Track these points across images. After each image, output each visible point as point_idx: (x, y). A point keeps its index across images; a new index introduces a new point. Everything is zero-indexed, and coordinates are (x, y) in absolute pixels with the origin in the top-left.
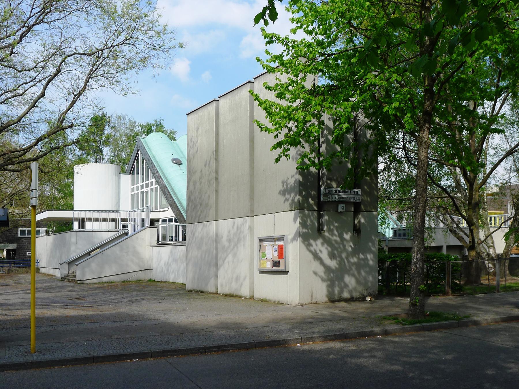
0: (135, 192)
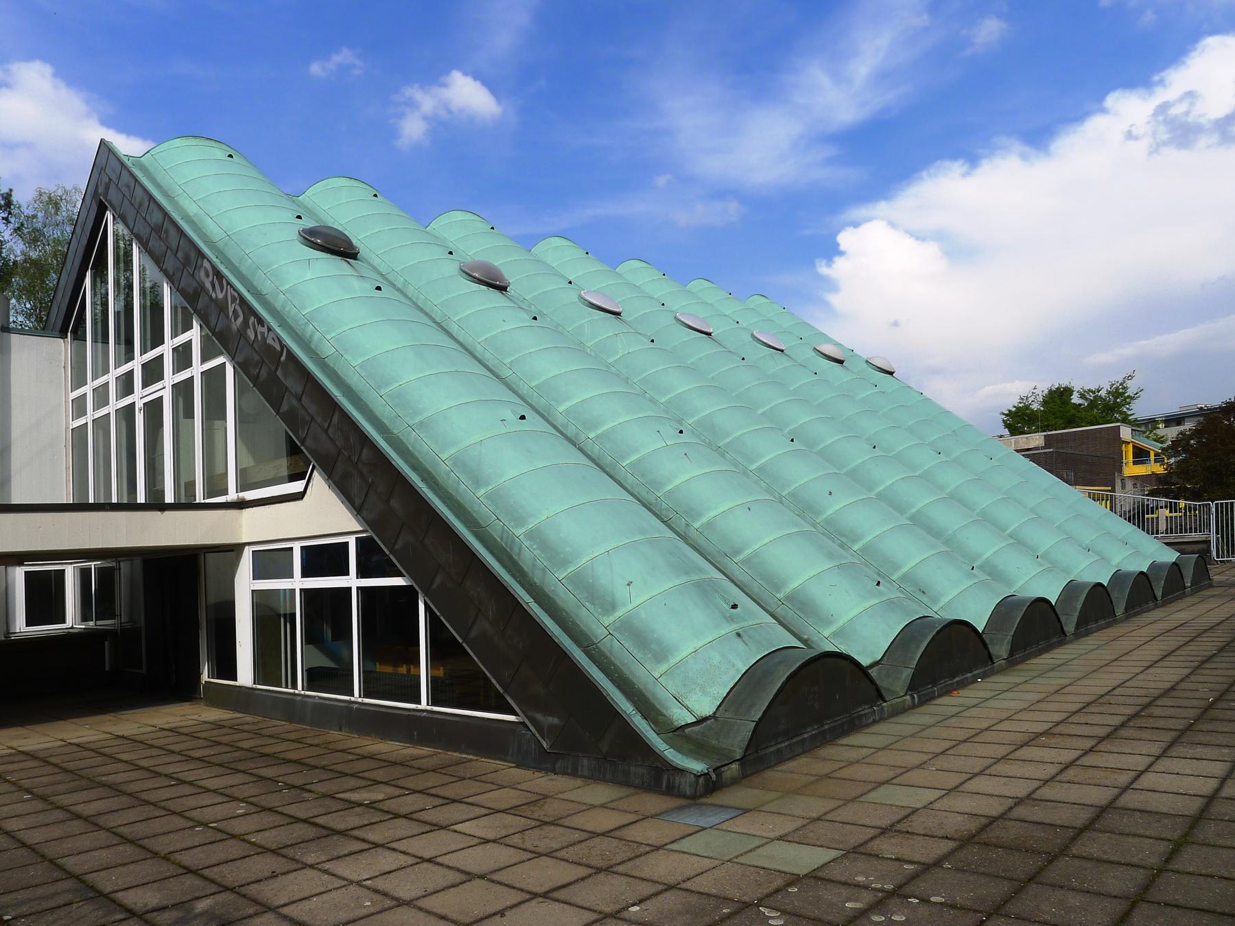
0: (91, 415)
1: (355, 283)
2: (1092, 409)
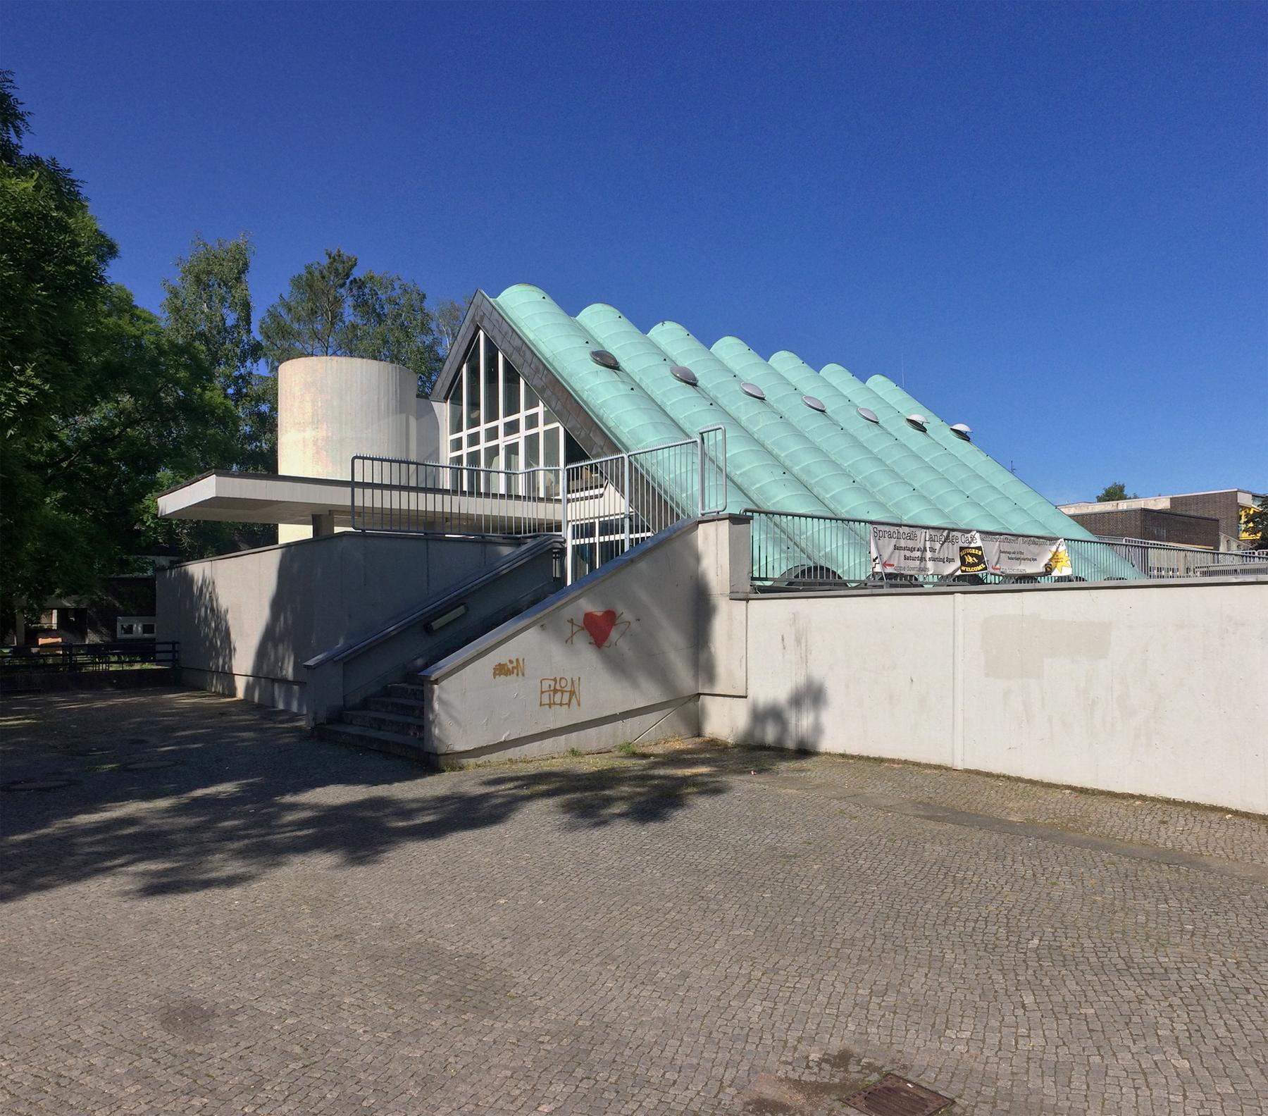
1: (621, 386)
2: (34, 609)
